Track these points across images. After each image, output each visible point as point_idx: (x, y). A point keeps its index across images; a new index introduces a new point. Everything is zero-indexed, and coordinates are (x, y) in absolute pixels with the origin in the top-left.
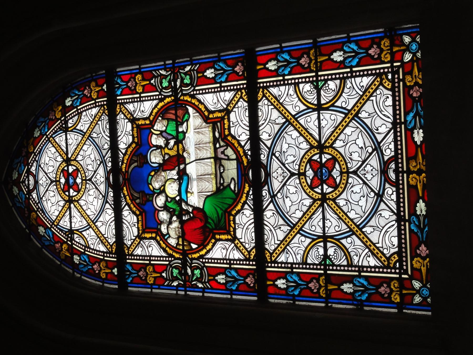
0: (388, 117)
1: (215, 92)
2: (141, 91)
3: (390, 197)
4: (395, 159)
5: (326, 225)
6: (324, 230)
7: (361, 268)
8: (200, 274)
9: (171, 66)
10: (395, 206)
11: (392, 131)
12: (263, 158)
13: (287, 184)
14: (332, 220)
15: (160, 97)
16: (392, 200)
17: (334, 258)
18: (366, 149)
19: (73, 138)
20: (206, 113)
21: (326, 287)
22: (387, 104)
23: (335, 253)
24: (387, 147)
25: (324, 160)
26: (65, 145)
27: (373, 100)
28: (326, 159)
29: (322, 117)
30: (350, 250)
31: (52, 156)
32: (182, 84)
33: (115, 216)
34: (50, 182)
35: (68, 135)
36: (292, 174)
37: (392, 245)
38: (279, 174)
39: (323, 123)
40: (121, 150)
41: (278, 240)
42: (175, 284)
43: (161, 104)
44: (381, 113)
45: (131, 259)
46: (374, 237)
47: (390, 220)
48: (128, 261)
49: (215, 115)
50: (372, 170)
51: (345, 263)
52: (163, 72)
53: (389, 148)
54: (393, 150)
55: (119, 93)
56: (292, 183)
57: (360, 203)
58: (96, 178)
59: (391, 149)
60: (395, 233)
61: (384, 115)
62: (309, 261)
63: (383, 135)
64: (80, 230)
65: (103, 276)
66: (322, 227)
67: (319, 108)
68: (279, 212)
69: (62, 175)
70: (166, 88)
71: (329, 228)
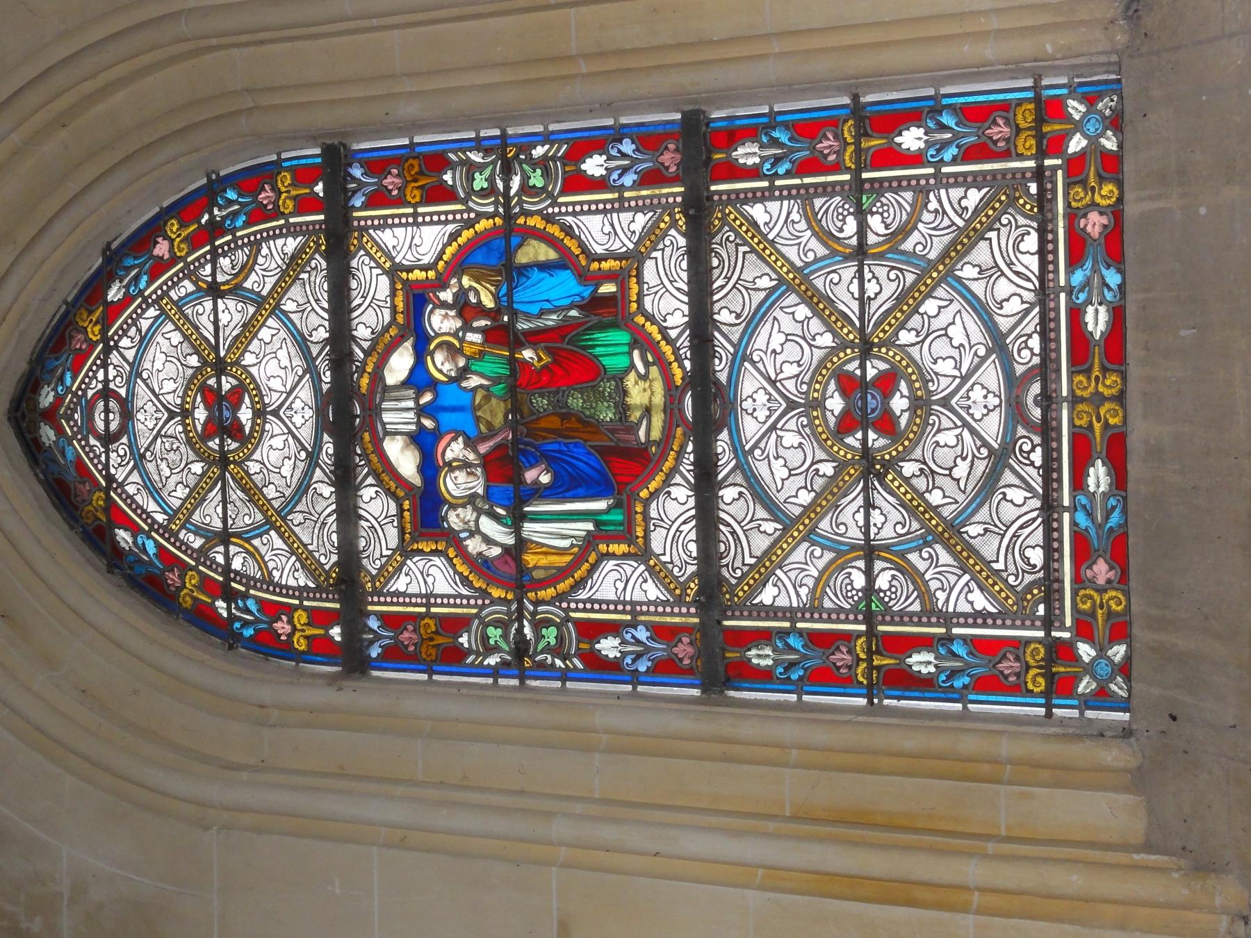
0: (1029, 280)
1: (605, 212)
2: (418, 199)
3: (1028, 458)
4: (1045, 369)
5: (872, 521)
6: (867, 533)
7: (948, 619)
8: (474, 179)
9: (499, 141)
10: (1040, 480)
11: (1037, 310)
12: (329, 447)
13: (284, 395)
14: (847, 298)
15: (465, 216)
16: (115, 367)
17: (890, 597)
18: (971, 348)
19: (232, 313)
20: (452, 553)
21: (869, 660)
22: (1023, 247)
23: (891, 586)
24: (1023, 345)
25: (226, 386)
26: (211, 329)
27: (656, 258)
28: (876, 371)
29: (868, 276)
30: (809, 233)
31: (172, 352)
32: (525, 189)
33: (698, 506)
34: (166, 415)
35: (219, 301)
36: (275, 413)
37: (1029, 564)
38: (300, 415)
39: (871, 288)
40: (362, 343)
41: (751, 556)
42: (492, 660)
43: (467, 234)
44: (1011, 269)
45: (379, 603)
46: (988, 548)
47: (1024, 509)
48: (370, 608)
49: (605, 265)
50: (985, 397)
51: (916, 607)
52: (476, 157)
53: (1027, 347)
54: (1037, 351)
55: (358, 201)
56: (792, 425)
57: (957, 473)
58: (290, 408)
59: (1031, 350)
60: (1038, 537)
61: (1017, 273)
62: (827, 604)
63: (1013, 320)
64: (246, 536)
65: (301, 645)
66: (861, 523)
67: (861, 253)
68: (758, 492)
69: (199, 399)
70: (483, 193)
71: (879, 529)
